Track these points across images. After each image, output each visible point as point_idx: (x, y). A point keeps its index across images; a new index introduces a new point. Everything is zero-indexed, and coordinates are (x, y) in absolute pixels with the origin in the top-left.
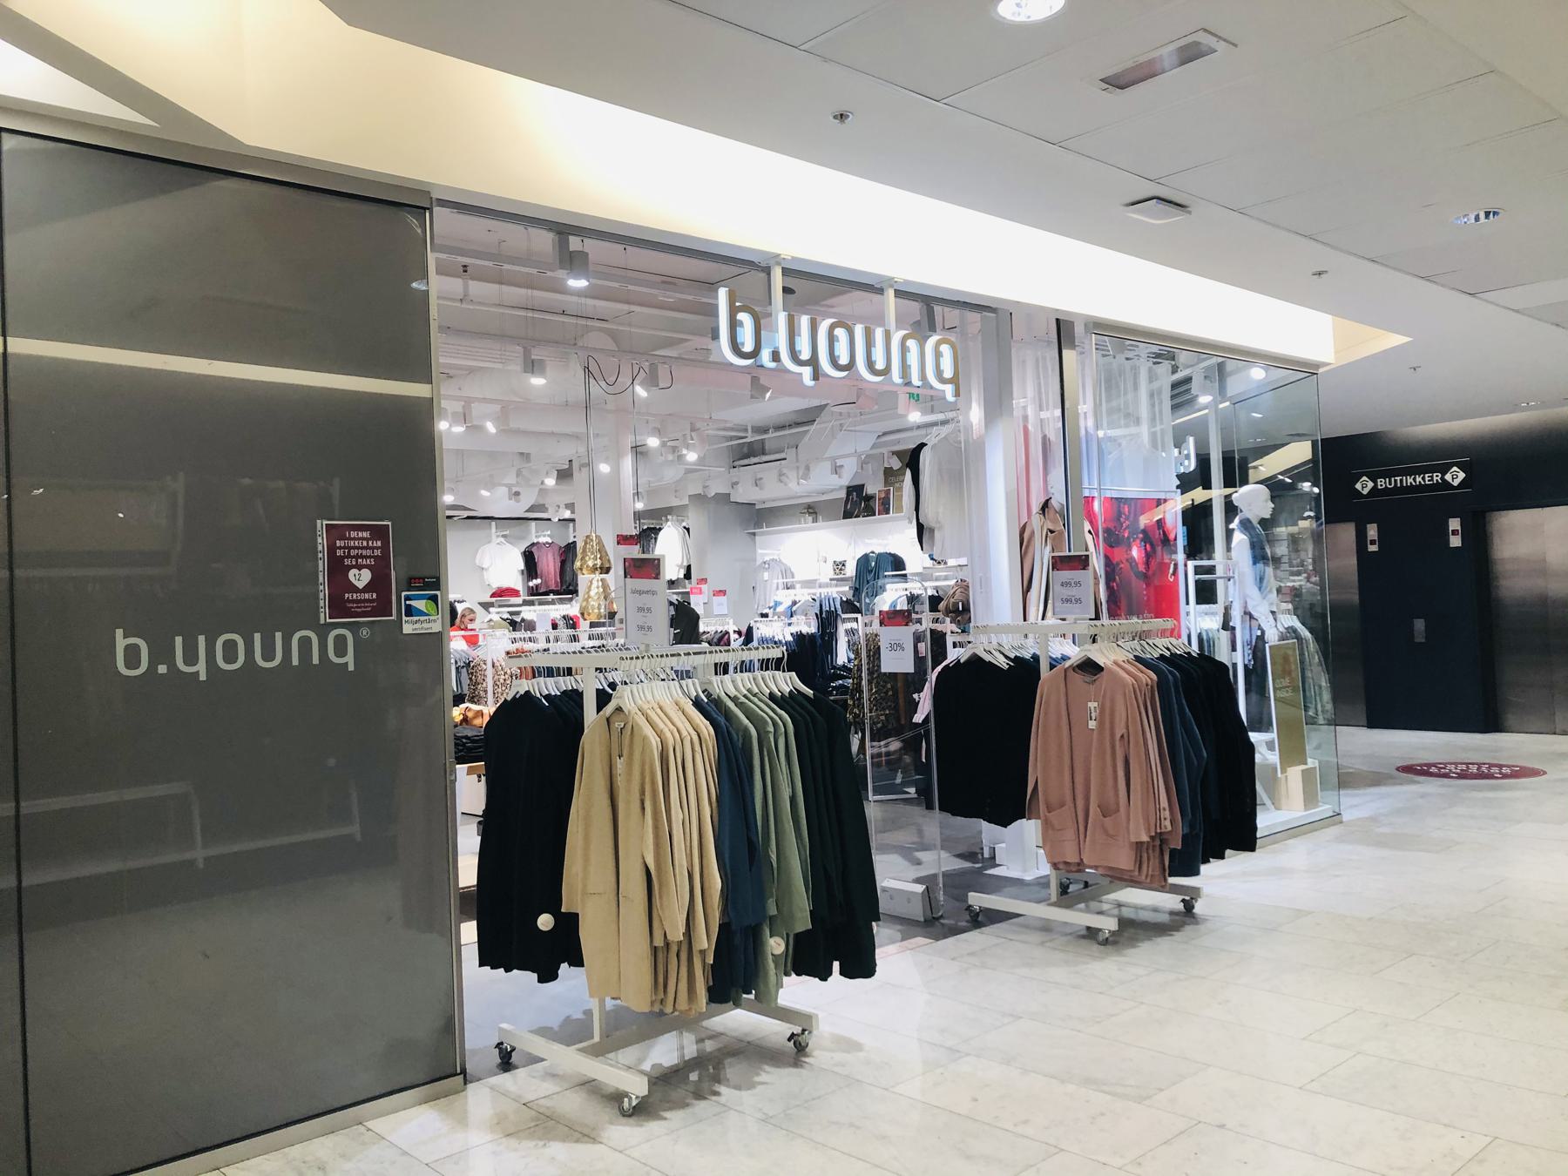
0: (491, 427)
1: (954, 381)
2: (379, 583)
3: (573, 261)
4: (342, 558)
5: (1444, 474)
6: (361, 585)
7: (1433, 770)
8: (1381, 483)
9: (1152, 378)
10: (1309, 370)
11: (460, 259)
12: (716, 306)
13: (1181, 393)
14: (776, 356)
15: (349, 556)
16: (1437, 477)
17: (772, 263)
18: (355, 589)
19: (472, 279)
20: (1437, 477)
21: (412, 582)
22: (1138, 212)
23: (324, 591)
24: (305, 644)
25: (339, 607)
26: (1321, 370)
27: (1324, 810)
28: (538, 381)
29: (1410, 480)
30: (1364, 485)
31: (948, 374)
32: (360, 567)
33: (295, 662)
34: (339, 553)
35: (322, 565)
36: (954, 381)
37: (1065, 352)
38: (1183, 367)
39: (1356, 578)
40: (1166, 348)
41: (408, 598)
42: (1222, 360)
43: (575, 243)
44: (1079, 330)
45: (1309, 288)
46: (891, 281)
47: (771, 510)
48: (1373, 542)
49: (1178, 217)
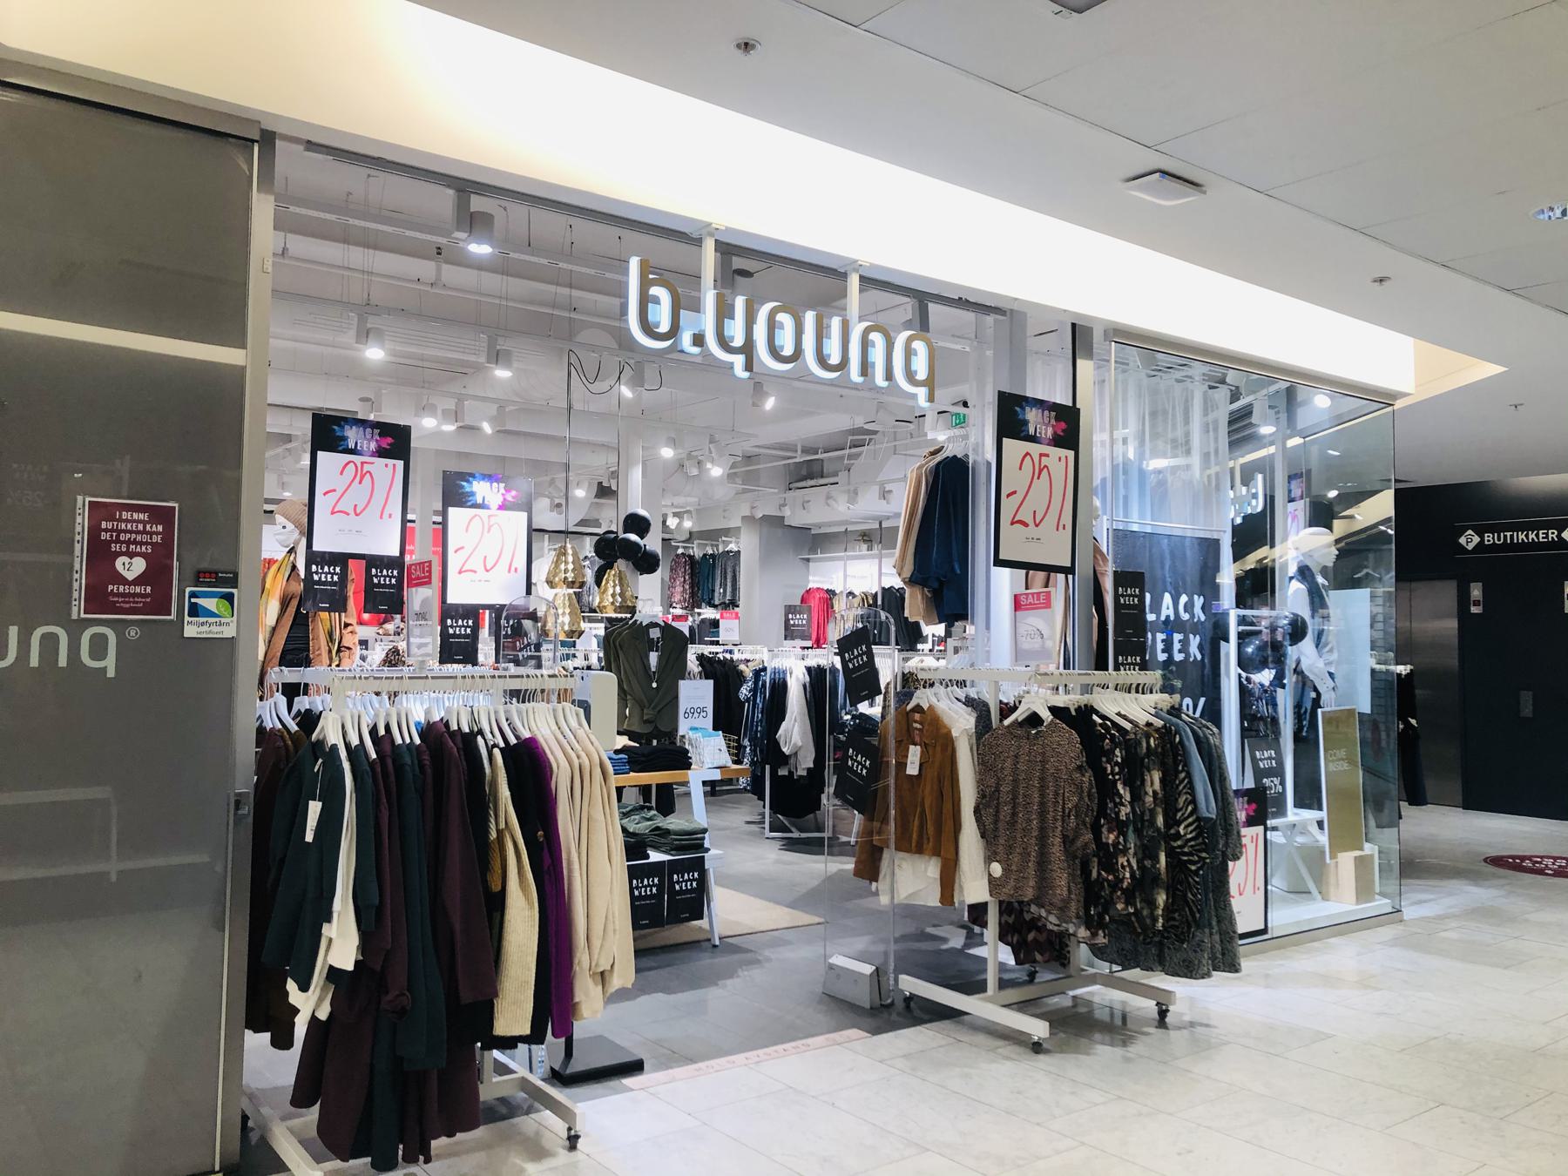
0: (487, 428)
1: (930, 383)
2: (157, 574)
3: (474, 223)
4: (108, 543)
5: (1560, 531)
6: (130, 576)
7: (1527, 863)
8: (1489, 538)
9: (1208, 407)
10: (1385, 398)
11: (434, 238)
12: (627, 284)
13: (1240, 427)
14: (699, 340)
15: (117, 541)
16: (1553, 534)
17: (704, 232)
18: (123, 581)
19: (447, 262)
20: (1553, 534)
21: (200, 577)
22: (1139, 189)
23: (80, 581)
24: (50, 642)
25: (98, 599)
26: (1399, 404)
27: (1381, 904)
28: (502, 373)
29: (1522, 536)
30: (1469, 540)
31: (922, 375)
32: (131, 555)
33: (34, 661)
34: (104, 536)
35: (80, 549)
36: (930, 383)
37: (1079, 362)
38: (1248, 397)
39: (1456, 641)
40: (1220, 367)
41: (193, 595)
42: (1289, 389)
43: (477, 203)
44: (1098, 336)
45: (1373, 297)
46: (854, 265)
47: (834, 535)
48: (1476, 603)
49: (1191, 198)
